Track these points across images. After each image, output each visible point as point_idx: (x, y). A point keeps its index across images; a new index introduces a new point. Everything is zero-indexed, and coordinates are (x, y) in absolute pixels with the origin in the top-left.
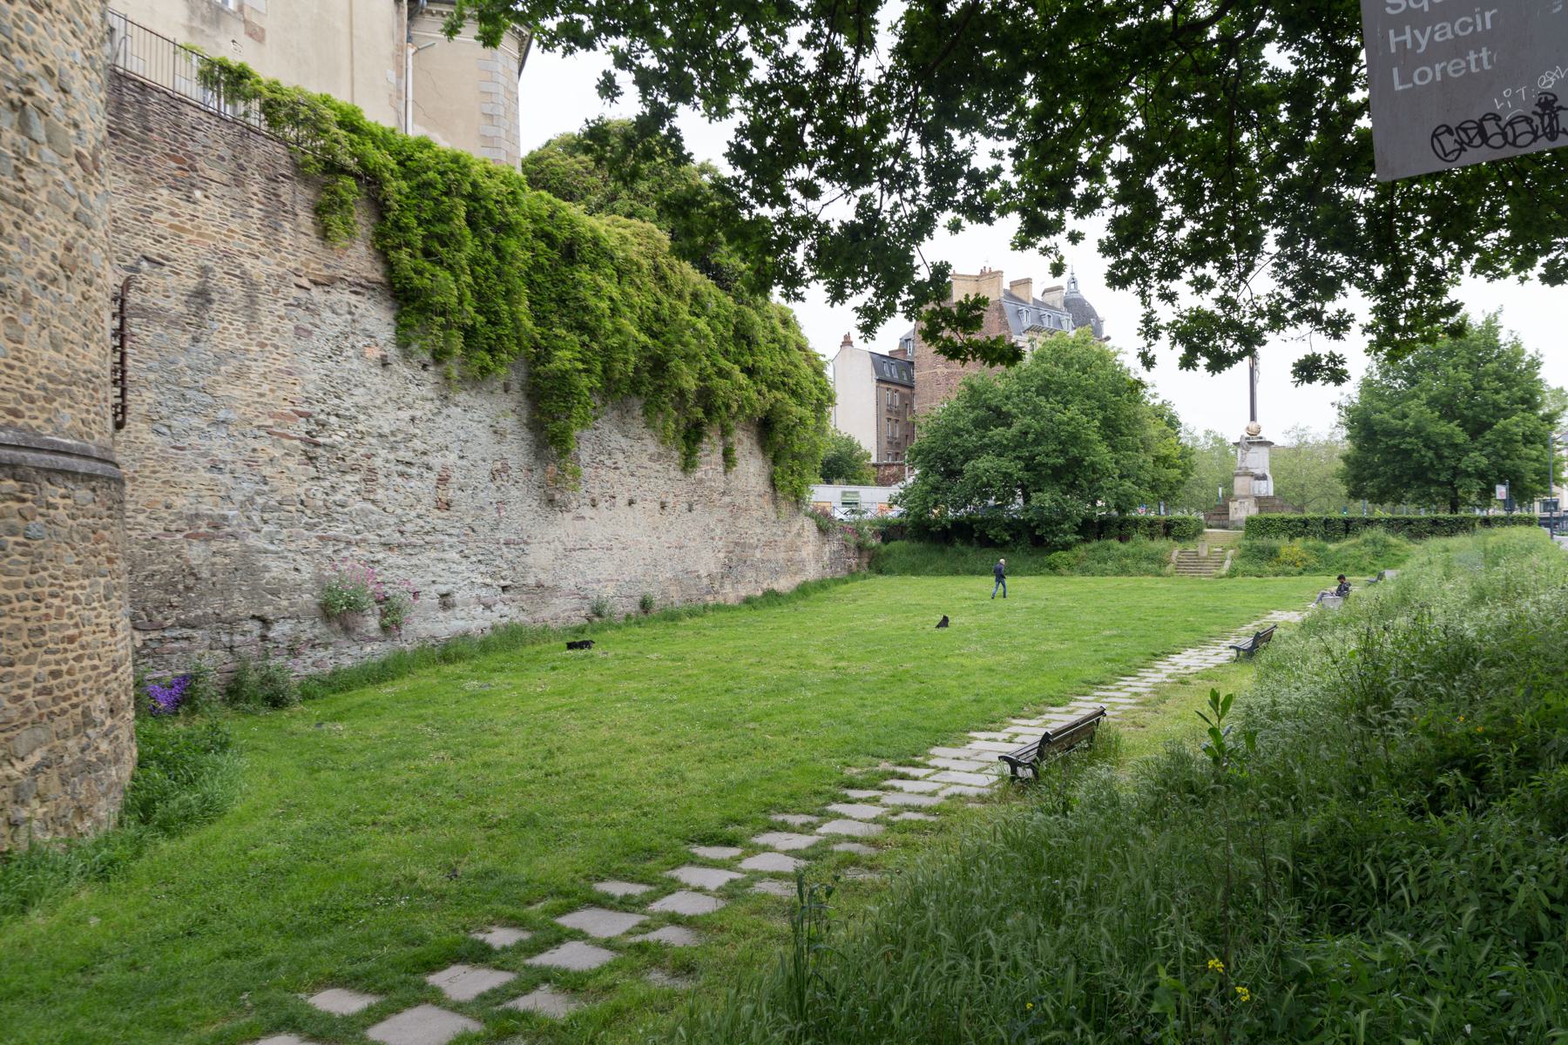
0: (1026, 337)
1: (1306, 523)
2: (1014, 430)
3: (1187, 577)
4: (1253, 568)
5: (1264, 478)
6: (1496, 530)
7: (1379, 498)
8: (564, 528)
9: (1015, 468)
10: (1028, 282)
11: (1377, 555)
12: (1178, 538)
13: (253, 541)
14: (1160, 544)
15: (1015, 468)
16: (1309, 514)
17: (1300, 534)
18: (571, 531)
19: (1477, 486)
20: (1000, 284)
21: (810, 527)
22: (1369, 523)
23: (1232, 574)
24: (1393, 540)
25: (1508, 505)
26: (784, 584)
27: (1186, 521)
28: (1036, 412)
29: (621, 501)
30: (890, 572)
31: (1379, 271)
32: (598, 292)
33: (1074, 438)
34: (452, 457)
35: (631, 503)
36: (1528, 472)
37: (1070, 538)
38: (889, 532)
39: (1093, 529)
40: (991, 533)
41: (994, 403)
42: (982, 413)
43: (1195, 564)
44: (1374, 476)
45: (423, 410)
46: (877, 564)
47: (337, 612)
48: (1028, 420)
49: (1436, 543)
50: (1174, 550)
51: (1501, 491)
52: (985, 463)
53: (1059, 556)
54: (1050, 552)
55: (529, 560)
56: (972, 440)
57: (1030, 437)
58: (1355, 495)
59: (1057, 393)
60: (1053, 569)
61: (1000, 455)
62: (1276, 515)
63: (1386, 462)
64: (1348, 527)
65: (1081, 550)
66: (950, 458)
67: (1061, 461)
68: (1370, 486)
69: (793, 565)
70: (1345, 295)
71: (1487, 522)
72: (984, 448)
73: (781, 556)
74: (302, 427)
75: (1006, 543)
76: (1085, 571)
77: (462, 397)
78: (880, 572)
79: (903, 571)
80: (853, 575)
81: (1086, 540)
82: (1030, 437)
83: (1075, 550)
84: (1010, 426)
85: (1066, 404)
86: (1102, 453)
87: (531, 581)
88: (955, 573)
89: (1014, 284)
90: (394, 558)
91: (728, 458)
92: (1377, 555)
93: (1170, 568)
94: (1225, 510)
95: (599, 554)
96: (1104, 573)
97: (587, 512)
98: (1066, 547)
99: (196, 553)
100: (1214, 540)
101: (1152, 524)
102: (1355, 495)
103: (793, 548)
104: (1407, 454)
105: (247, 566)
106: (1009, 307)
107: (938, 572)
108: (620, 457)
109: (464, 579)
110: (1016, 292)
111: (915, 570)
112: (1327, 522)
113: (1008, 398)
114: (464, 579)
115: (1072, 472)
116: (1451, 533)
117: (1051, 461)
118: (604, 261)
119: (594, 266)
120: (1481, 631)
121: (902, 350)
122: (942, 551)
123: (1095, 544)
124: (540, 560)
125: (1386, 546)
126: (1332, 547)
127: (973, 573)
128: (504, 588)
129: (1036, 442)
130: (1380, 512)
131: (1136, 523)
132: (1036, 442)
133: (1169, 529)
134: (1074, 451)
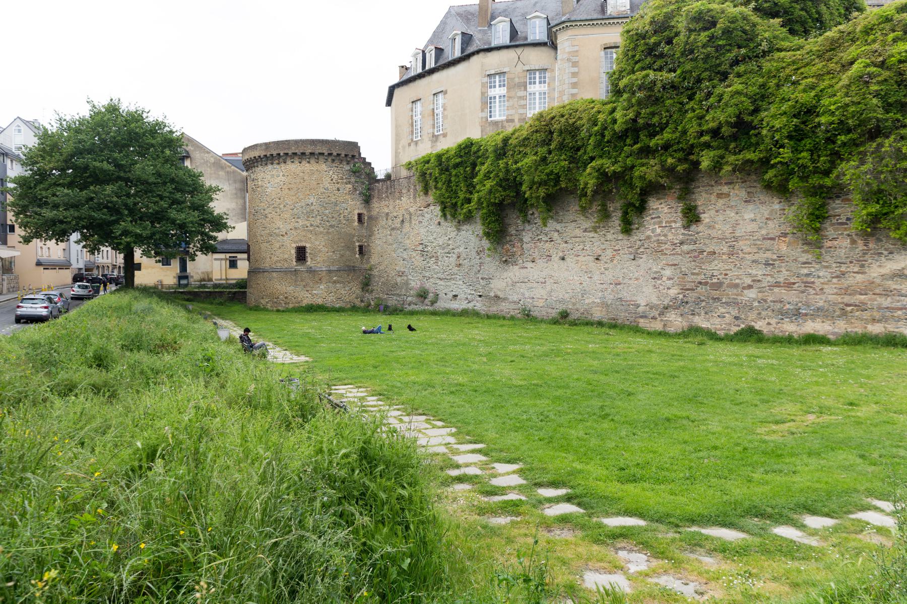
8: (514, 273)
13: (410, 277)
18: (517, 274)
29: (555, 258)
34: (462, 249)
45: (453, 234)
47: (423, 295)
55: (492, 286)
74: (420, 248)
77: (464, 227)
87: (492, 294)
90: (442, 283)
95: (535, 285)
97: (530, 265)
99: (399, 279)
105: (407, 283)
109: (463, 290)
114: (463, 290)
116: (847, 334)
120: (450, 544)
124: (498, 285)
128: (480, 296)
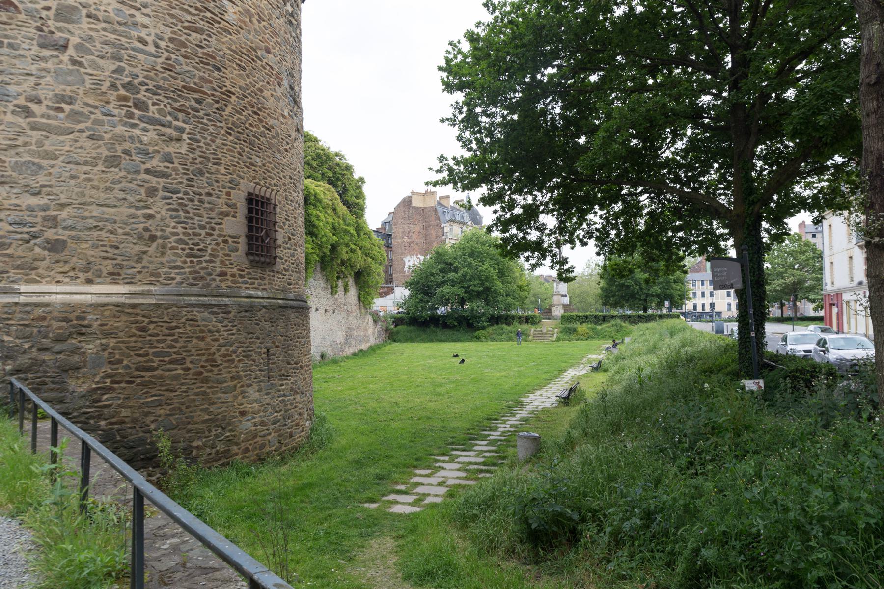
0: (447, 225)
1: (587, 317)
2: (459, 274)
3: (538, 341)
4: (567, 337)
5: (565, 296)
6: (665, 320)
7: (615, 305)
9: (461, 292)
10: (448, 197)
11: (618, 331)
12: (532, 324)
14: (525, 327)
15: (461, 292)
16: (588, 313)
17: (585, 322)
19: (656, 300)
20: (435, 198)
21: (370, 318)
22: (613, 317)
23: (558, 340)
24: (624, 325)
25: (670, 309)
26: (364, 347)
27: (535, 316)
28: (469, 266)
30: (399, 341)
31: (666, 256)
32: (318, 217)
33: (487, 278)
35: (317, 310)
36: (676, 294)
37: (485, 324)
38: (398, 321)
39: (496, 320)
40: (449, 322)
41: (449, 261)
42: (443, 265)
43: (541, 336)
44: (614, 296)
46: (392, 336)
48: (466, 269)
49: (642, 326)
50: (532, 330)
51: (667, 303)
52: (447, 289)
53: (480, 333)
54: (476, 331)
56: (439, 278)
57: (468, 278)
58: (604, 304)
59: (478, 257)
60: (478, 339)
61: (453, 286)
62: (574, 313)
63: (619, 290)
64: (604, 319)
65: (490, 330)
66: (429, 287)
67: (481, 288)
68: (612, 300)
69: (366, 338)
70: (440, 69)
71: (661, 317)
72: (444, 283)
73: (362, 333)
75: (455, 326)
76: (492, 340)
78: (395, 341)
79: (406, 341)
80: (385, 343)
81: (492, 325)
82: (468, 278)
83: (487, 330)
84: (457, 272)
85: (483, 262)
86: (498, 285)
88: (431, 341)
89: (441, 198)
91: (346, 290)
92: (618, 331)
93: (531, 338)
94: (550, 310)
96: (501, 340)
98: (483, 328)
100: (547, 325)
101: (520, 317)
102: (604, 304)
103: (366, 330)
104: (628, 287)
106: (440, 209)
107: (423, 341)
108: (313, 289)
110: (442, 202)
111: (412, 340)
112: (596, 316)
113: (455, 258)
115: (486, 294)
117: (477, 289)
118: (318, 204)
119: (315, 206)
121: (383, 228)
122: (424, 331)
123: (496, 327)
125: (621, 327)
126: (599, 328)
127: (440, 341)
129: (470, 280)
130: (613, 312)
131: (513, 317)
132: (470, 280)
133: (528, 320)
134: (487, 284)
